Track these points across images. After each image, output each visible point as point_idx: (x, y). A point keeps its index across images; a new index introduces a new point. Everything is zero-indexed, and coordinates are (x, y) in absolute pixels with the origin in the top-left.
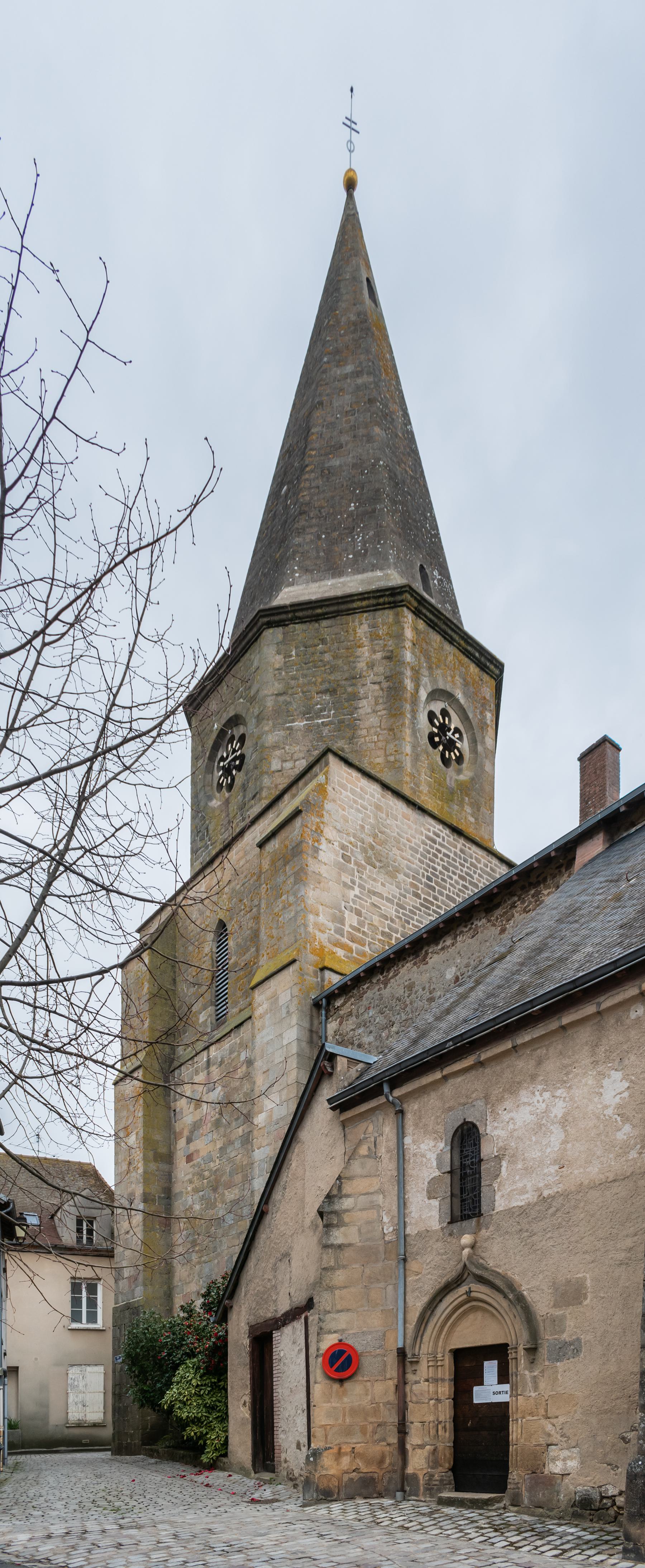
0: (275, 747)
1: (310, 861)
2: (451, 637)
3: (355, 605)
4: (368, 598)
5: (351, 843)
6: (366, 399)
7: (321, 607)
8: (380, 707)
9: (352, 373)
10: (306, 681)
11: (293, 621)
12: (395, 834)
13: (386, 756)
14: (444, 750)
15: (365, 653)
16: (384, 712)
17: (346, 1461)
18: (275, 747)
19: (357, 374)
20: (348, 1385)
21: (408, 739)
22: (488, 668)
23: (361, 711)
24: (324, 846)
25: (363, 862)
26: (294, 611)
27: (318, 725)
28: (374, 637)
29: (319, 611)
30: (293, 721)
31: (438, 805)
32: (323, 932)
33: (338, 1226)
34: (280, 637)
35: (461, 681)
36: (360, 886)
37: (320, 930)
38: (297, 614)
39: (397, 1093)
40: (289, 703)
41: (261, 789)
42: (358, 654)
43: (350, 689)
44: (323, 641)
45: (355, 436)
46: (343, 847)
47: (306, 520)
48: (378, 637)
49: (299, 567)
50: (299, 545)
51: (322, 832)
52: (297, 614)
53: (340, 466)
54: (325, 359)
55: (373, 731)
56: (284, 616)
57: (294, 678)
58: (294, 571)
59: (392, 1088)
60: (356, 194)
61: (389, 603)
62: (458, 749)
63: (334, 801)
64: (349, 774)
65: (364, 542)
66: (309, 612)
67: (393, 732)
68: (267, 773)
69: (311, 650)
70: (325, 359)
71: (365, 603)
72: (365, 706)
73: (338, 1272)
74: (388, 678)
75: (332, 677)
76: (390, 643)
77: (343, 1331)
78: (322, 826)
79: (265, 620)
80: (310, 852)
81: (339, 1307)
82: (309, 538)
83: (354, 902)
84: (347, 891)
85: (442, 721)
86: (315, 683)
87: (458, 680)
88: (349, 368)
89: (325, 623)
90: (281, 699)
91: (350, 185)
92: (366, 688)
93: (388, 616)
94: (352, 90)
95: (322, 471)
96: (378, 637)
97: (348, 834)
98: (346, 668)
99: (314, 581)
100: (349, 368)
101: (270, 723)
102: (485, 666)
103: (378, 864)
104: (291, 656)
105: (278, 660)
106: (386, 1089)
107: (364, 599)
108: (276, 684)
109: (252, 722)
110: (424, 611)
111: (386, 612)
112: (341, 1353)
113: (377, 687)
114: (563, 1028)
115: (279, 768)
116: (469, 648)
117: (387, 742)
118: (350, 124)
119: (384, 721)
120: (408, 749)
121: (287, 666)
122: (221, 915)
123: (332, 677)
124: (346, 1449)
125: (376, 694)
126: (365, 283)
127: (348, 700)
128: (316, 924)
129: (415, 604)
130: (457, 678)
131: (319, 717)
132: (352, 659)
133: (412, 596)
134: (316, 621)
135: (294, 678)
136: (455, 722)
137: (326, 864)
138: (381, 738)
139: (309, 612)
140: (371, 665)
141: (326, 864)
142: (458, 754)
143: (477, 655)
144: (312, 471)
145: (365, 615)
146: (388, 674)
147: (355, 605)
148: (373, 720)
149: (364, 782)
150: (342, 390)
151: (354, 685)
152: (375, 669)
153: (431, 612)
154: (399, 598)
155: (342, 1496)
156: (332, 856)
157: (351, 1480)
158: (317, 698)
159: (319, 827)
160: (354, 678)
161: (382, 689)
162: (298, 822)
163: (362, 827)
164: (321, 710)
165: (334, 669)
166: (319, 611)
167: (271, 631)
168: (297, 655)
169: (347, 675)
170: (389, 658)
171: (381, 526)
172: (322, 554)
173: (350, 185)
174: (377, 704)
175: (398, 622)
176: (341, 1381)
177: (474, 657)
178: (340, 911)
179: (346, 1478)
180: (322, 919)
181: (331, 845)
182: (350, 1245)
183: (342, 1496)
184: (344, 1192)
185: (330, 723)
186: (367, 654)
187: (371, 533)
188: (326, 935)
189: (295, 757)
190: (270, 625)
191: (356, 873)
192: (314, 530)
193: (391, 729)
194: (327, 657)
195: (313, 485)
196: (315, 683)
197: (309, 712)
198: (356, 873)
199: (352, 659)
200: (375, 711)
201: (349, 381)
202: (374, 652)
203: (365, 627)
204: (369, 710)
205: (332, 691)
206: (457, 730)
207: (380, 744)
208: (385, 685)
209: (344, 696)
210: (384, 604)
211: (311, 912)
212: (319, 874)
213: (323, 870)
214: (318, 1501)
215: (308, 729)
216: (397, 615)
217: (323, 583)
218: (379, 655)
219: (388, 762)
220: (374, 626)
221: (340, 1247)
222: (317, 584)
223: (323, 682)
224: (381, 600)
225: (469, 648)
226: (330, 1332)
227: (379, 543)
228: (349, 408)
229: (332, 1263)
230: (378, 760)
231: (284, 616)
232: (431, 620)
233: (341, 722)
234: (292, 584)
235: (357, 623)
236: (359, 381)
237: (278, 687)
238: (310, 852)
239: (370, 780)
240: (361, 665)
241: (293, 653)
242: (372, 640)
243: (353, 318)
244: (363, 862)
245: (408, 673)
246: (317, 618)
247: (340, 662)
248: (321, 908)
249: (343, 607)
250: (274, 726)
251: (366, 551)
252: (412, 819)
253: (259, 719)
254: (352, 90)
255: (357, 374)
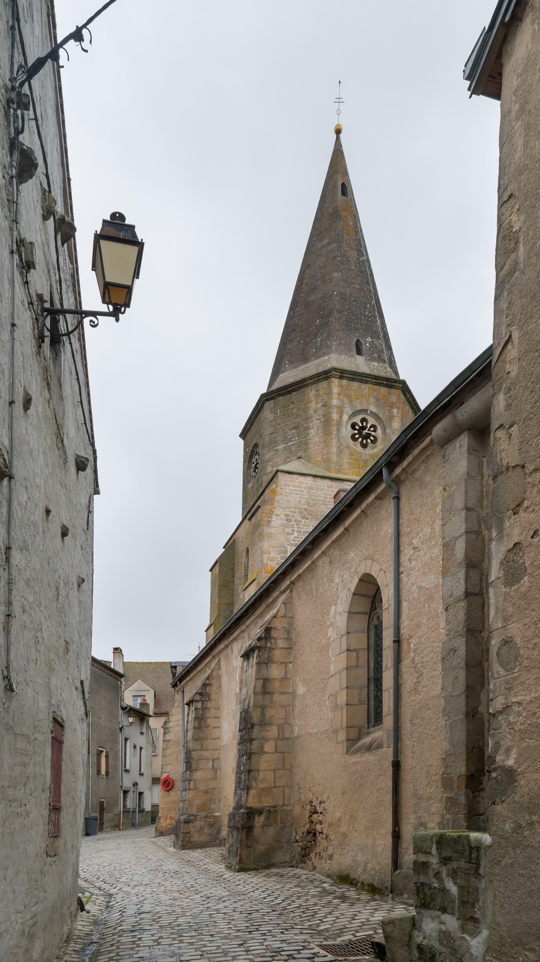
0: (269, 460)
1: (265, 528)
2: (366, 381)
3: (307, 382)
4: (314, 378)
5: (292, 512)
6: (332, 258)
7: (291, 387)
8: (320, 431)
9: (327, 244)
10: (284, 424)
11: (279, 395)
12: (323, 498)
13: (322, 456)
14: (362, 440)
15: (313, 405)
16: (322, 434)
17: (168, 820)
18: (269, 460)
19: (329, 244)
20: (170, 792)
21: (334, 444)
22: (394, 386)
23: (311, 435)
24: (274, 518)
25: (300, 519)
26: (278, 392)
27: (290, 446)
28: (317, 396)
29: (290, 389)
30: (278, 446)
31: (356, 472)
32: (272, 561)
33: (168, 733)
34: (272, 404)
35: (374, 400)
36: (298, 531)
37: (271, 561)
38: (280, 393)
39: (182, 684)
40: (275, 437)
41: (263, 482)
42: (309, 406)
43: (305, 425)
44: (293, 403)
45: (324, 281)
46: (286, 515)
47: (295, 334)
48: (320, 396)
49: (288, 361)
50: (290, 349)
51: (273, 512)
52: (280, 393)
53: (315, 299)
54: (314, 239)
55: (316, 444)
56: (273, 395)
57: (279, 424)
58: (286, 364)
59: (180, 683)
60: (341, 136)
61: (325, 378)
62: (373, 436)
63: (281, 494)
64: (291, 478)
65: (321, 341)
66: (286, 391)
67: (326, 443)
68: (265, 474)
69: (286, 408)
70: (314, 239)
71: (312, 381)
72: (312, 432)
73: (168, 750)
74: (324, 416)
75: (297, 421)
76: (325, 398)
77: (169, 772)
78: (273, 509)
79: (265, 398)
80: (265, 524)
81: (168, 763)
82: (295, 344)
83: (293, 540)
84: (288, 536)
85: (361, 425)
86: (288, 425)
87: (372, 400)
88: (325, 242)
89: (293, 394)
90: (272, 436)
91: (338, 132)
92: (313, 423)
93: (325, 384)
94: (340, 82)
95: (306, 305)
96: (320, 396)
97: (290, 508)
98: (303, 414)
99: (295, 368)
100: (325, 242)
101: (267, 449)
102: (392, 385)
103: (310, 517)
104: (277, 413)
105: (271, 417)
106: (178, 683)
107: (312, 379)
108: (270, 429)
109: (260, 447)
110: (345, 375)
111: (324, 382)
112: (167, 780)
113: (318, 421)
114: (199, 671)
115: (271, 471)
116: (379, 381)
117: (323, 449)
118: (339, 101)
119: (322, 438)
120: (334, 450)
121: (275, 419)
122: (247, 546)
123: (297, 421)
124: (169, 816)
125: (318, 425)
126: (340, 187)
127: (304, 431)
128: (269, 559)
129: (339, 374)
130: (371, 399)
131: (290, 442)
132: (306, 409)
133: (336, 371)
134: (289, 393)
135: (279, 424)
136: (371, 421)
137: (275, 527)
138: (320, 447)
139: (286, 391)
140: (316, 411)
141: (275, 527)
142: (372, 438)
143: (385, 382)
144: (301, 306)
145: (313, 386)
146: (324, 414)
147: (307, 382)
148: (317, 439)
149: (301, 478)
150: (320, 255)
151: (307, 422)
152: (318, 412)
153: (350, 374)
154: (329, 374)
155: (167, 834)
156: (280, 522)
157: (170, 828)
158: (289, 432)
159: (271, 511)
160: (308, 419)
161: (321, 422)
162: (260, 510)
163: (300, 501)
164: (291, 438)
165: (298, 416)
166: (290, 389)
167: (268, 403)
168: (280, 412)
169: (304, 418)
170: (324, 405)
171: (331, 330)
172: (300, 352)
173: (338, 132)
174: (318, 430)
175: (329, 386)
176: (168, 791)
177: (383, 384)
178: (285, 547)
179: (168, 827)
180: (272, 554)
181: (279, 517)
182: (171, 740)
183: (167, 834)
184: (170, 720)
185: (296, 444)
186: (314, 406)
187: (325, 335)
188: (275, 562)
189: (279, 464)
190: (267, 400)
191: (295, 526)
192: (297, 339)
193: (325, 442)
194: (295, 411)
195: (300, 313)
196: (288, 425)
197: (285, 440)
198: (295, 526)
199: (306, 409)
200: (317, 434)
201: (324, 249)
202: (317, 404)
203: (313, 392)
204: (315, 434)
205: (296, 428)
206: (372, 426)
207: (320, 450)
208: (322, 420)
209: (302, 429)
210: (322, 379)
211: (266, 553)
212: (271, 533)
213: (274, 531)
214: (159, 836)
215: (285, 449)
216: (329, 383)
217: (298, 368)
218: (320, 405)
219: (324, 459)
220: (317, 391)
221: (168, 741)
222: (295, 370)
223: (292, 423)
224: (320, 377)
225: (379, 381)
226: (165, 773)
227: (329, 340)
228: (323, 265)
229: (166, 747)
230: (319, 459)
231: (273, 395)
232: (350, 378)
233: (301, 442)
234: (284, 372)
235: (309, 391)
236: (330, 248)
237: (271, 430)
238: (265, 524)
239: (305, 476)
240: (311, 412)
241: (279, 412)
242: (316, 398)
243: (330, 211)
244: (300, 519)
245: (335, 410)
246: (290, 392)
247: (300, 412)
248: (272, 550)
249: (302, 385)
250: (269, 450)
251: (322, 346)
252: (334, 487)
253: (263, 447)
254: (340, 82)
255: (329, 244)
